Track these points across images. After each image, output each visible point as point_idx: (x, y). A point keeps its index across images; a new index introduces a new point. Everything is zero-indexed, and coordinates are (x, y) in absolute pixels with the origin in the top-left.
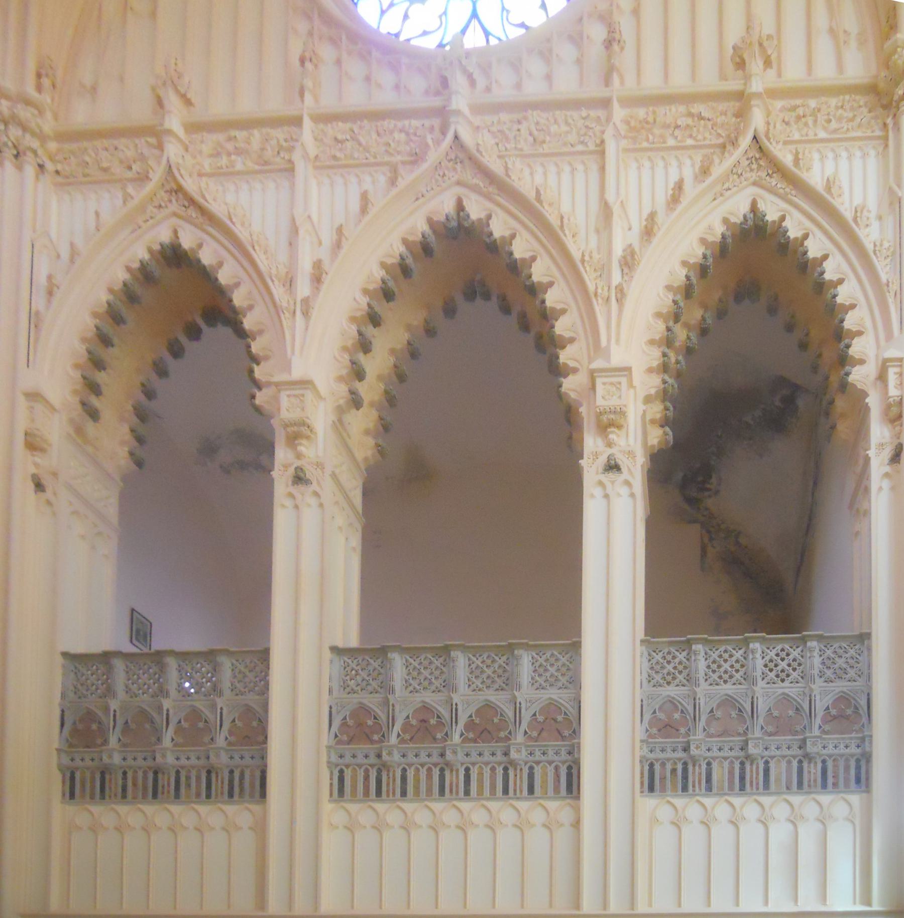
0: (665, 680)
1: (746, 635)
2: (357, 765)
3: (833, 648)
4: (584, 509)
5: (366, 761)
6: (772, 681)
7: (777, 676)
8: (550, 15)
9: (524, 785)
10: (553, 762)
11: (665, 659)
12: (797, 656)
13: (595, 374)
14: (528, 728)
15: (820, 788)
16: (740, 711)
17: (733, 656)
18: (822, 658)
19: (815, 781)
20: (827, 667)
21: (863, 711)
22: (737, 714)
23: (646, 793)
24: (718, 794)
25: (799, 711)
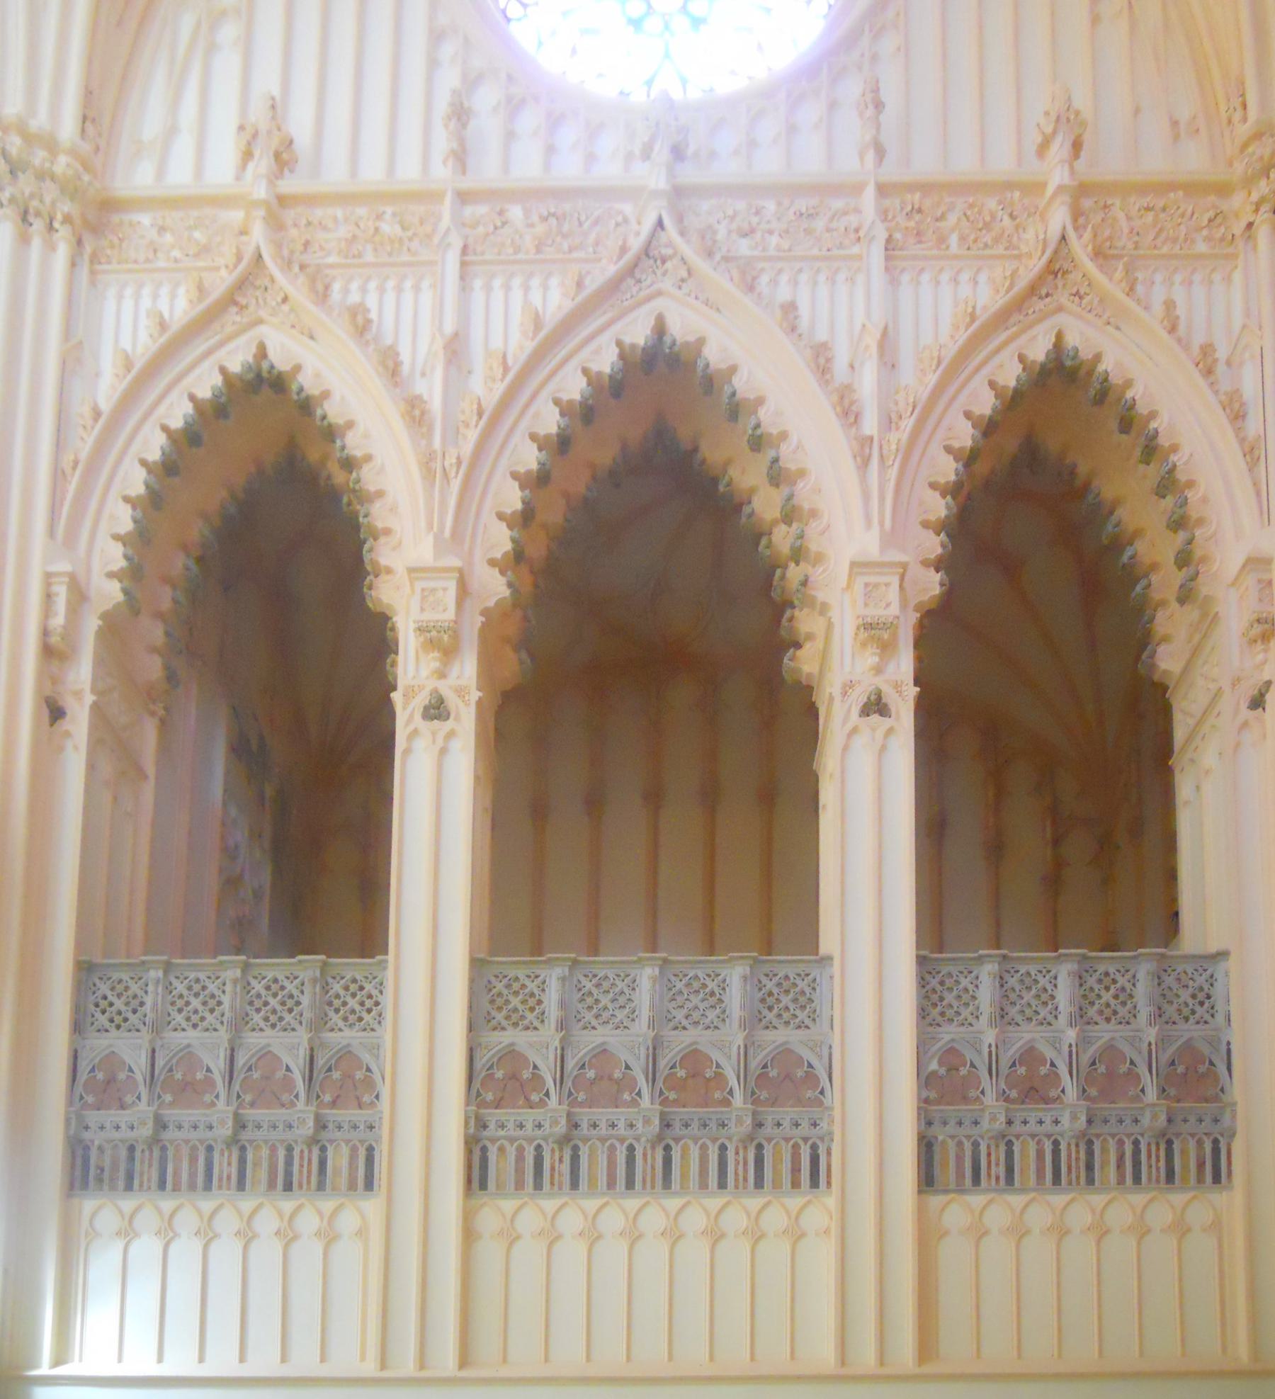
0: (355, 1024)
1: (731, 954)
2: (618, 1139)
3: (1176, 973)
4: (913, 802)
5: (502, 1133)
6: (298, 1017)
7: (290, 1011)
8: (652, 97)
9: (641, 1169)
10: (791, 1139)
11: (122, 994)
12: (683, 982)
13: (54, 580)
14: (729, 1099)
15: (660, 1188)
16: (250, 1069)
17: (713, 992)
18: (925, 990)
19: (229, 1177)
20: (126, 991)
21: (1221, 1068)
22: (256, 1071)
23: (1162, 1184)
24: (1181, 1188)
25: (251, 1066)
